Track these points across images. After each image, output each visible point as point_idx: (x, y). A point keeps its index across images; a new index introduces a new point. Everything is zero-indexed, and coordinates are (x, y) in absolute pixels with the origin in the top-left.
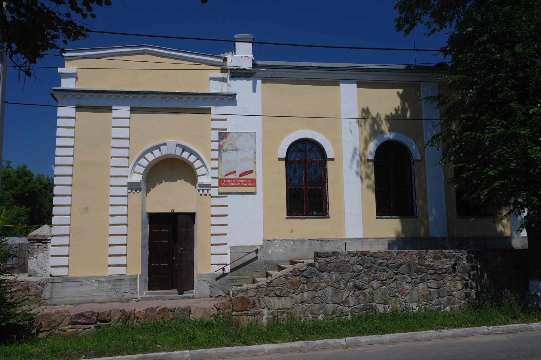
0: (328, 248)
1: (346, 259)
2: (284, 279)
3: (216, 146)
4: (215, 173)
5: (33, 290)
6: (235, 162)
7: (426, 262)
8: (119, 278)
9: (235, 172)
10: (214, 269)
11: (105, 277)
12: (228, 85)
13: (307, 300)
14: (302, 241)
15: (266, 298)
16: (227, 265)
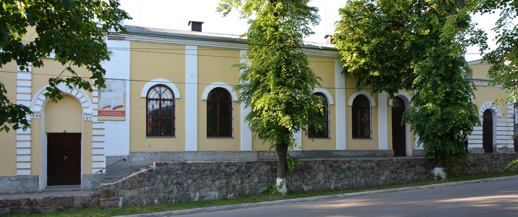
1: (173, 167)
2: (133, 179)
4: (96, 106)
7: (221, 169)
9: (110, 106)
10: (94, 171)
11: (14, 177)
14: (156, 153)
15: (122, 190)
16: (104, 168)
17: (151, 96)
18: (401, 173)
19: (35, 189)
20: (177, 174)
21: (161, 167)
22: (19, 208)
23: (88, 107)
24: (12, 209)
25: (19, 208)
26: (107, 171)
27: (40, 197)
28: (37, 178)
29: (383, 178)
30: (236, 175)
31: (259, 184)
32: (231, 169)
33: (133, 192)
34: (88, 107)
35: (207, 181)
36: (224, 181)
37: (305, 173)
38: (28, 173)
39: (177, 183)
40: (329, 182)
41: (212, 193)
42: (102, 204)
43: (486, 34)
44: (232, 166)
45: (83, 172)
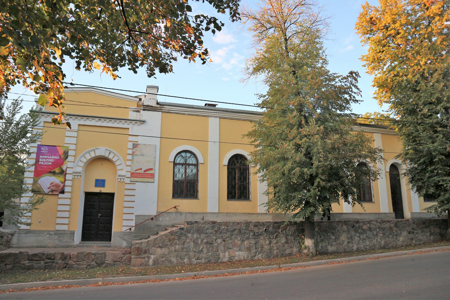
0: (197, 218)
1: (203, 226)
3: (130, 152)
4: (129, 169)
5: (5, 238)
6: (142, 164)
8: (63, 232)
9: (141, 169)
10: (124, 229)
11: (53, 231)
12: (141, 115)
13: (178, 250)
15: (153, 248)
17: (178, 161)
18: (417, 233)
19: (71, 244)
20: (207, 233)
21: (192, 226)
22: (54, 262)
23: (122, 169)
24: (46, 263)
25: (54, 262)
26: (135, 229)
27: (73, 252)
28: (73, 233)
29: (401, 239)
30: (264, 235)
31: (286, 245)
32: (259, 229)
33: (164, 251)
34: (122, 169)
35: (236, 241)
36: (253, 242)
37: (329, 234)
38: (65, 228)
39: (207, 243)
40: (352, 243)
41: (241, 253)
42: (133, 261)
43: (214, 32)
44: (260, 226)
45: (114, 229)
